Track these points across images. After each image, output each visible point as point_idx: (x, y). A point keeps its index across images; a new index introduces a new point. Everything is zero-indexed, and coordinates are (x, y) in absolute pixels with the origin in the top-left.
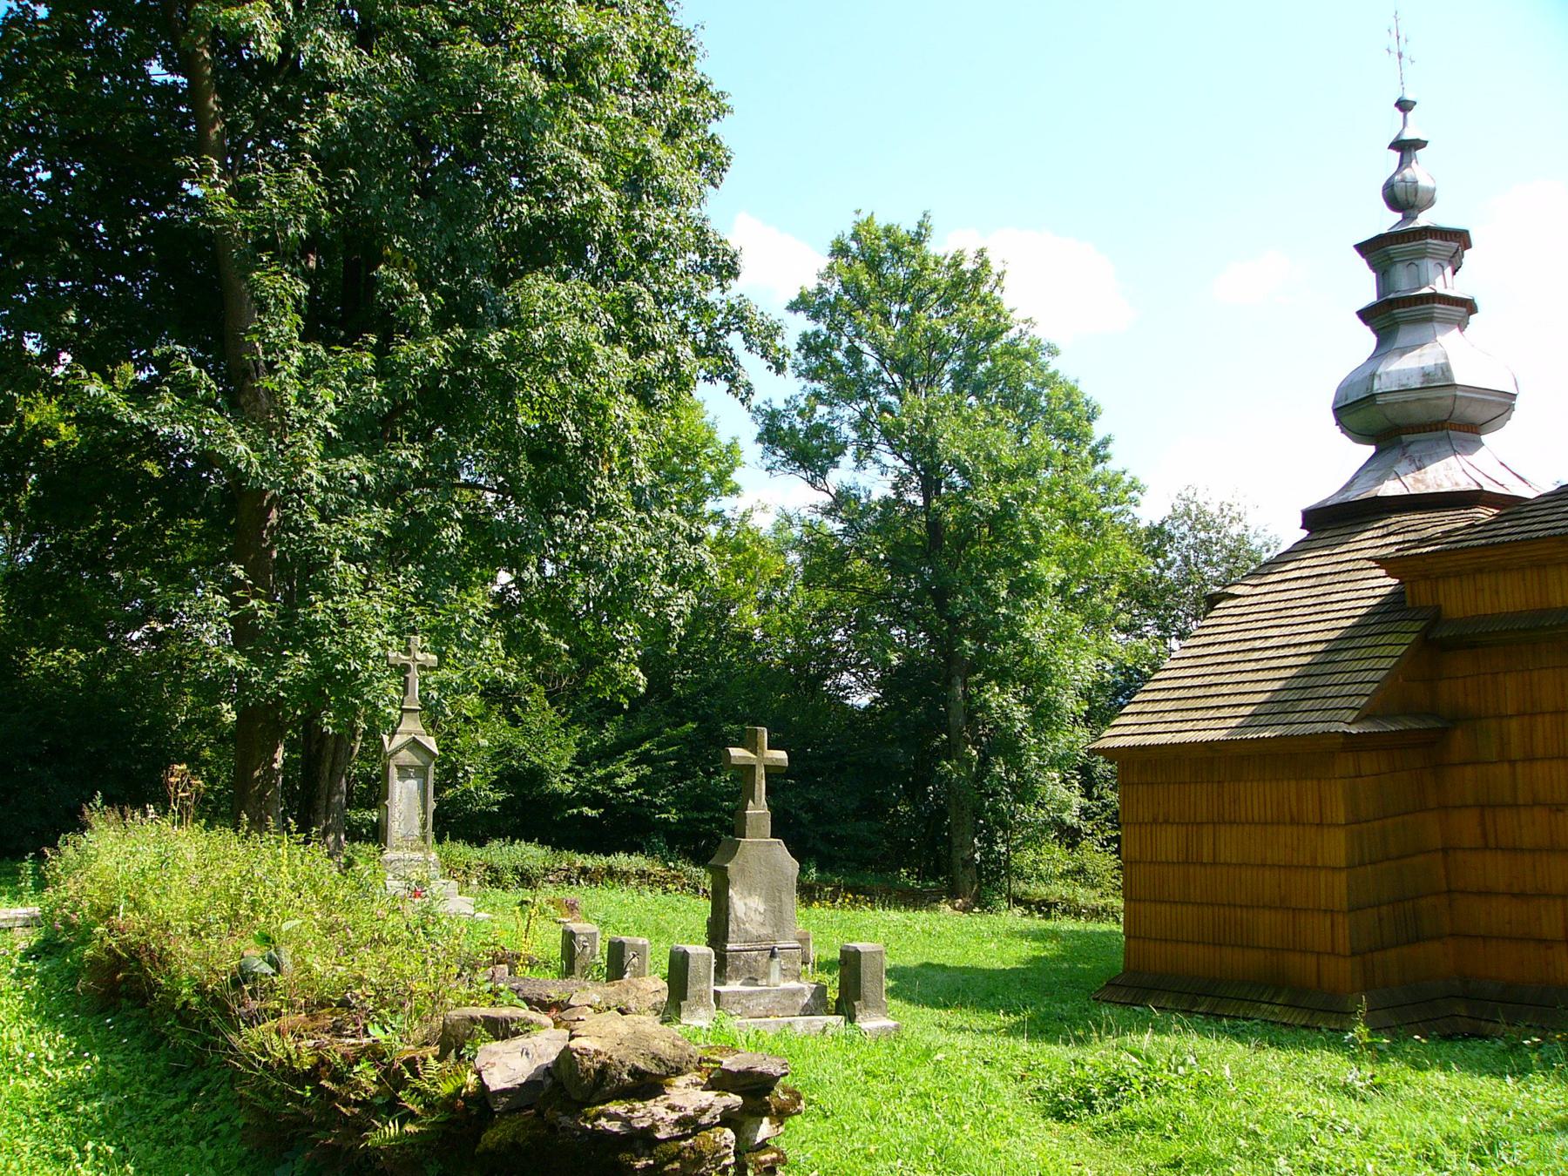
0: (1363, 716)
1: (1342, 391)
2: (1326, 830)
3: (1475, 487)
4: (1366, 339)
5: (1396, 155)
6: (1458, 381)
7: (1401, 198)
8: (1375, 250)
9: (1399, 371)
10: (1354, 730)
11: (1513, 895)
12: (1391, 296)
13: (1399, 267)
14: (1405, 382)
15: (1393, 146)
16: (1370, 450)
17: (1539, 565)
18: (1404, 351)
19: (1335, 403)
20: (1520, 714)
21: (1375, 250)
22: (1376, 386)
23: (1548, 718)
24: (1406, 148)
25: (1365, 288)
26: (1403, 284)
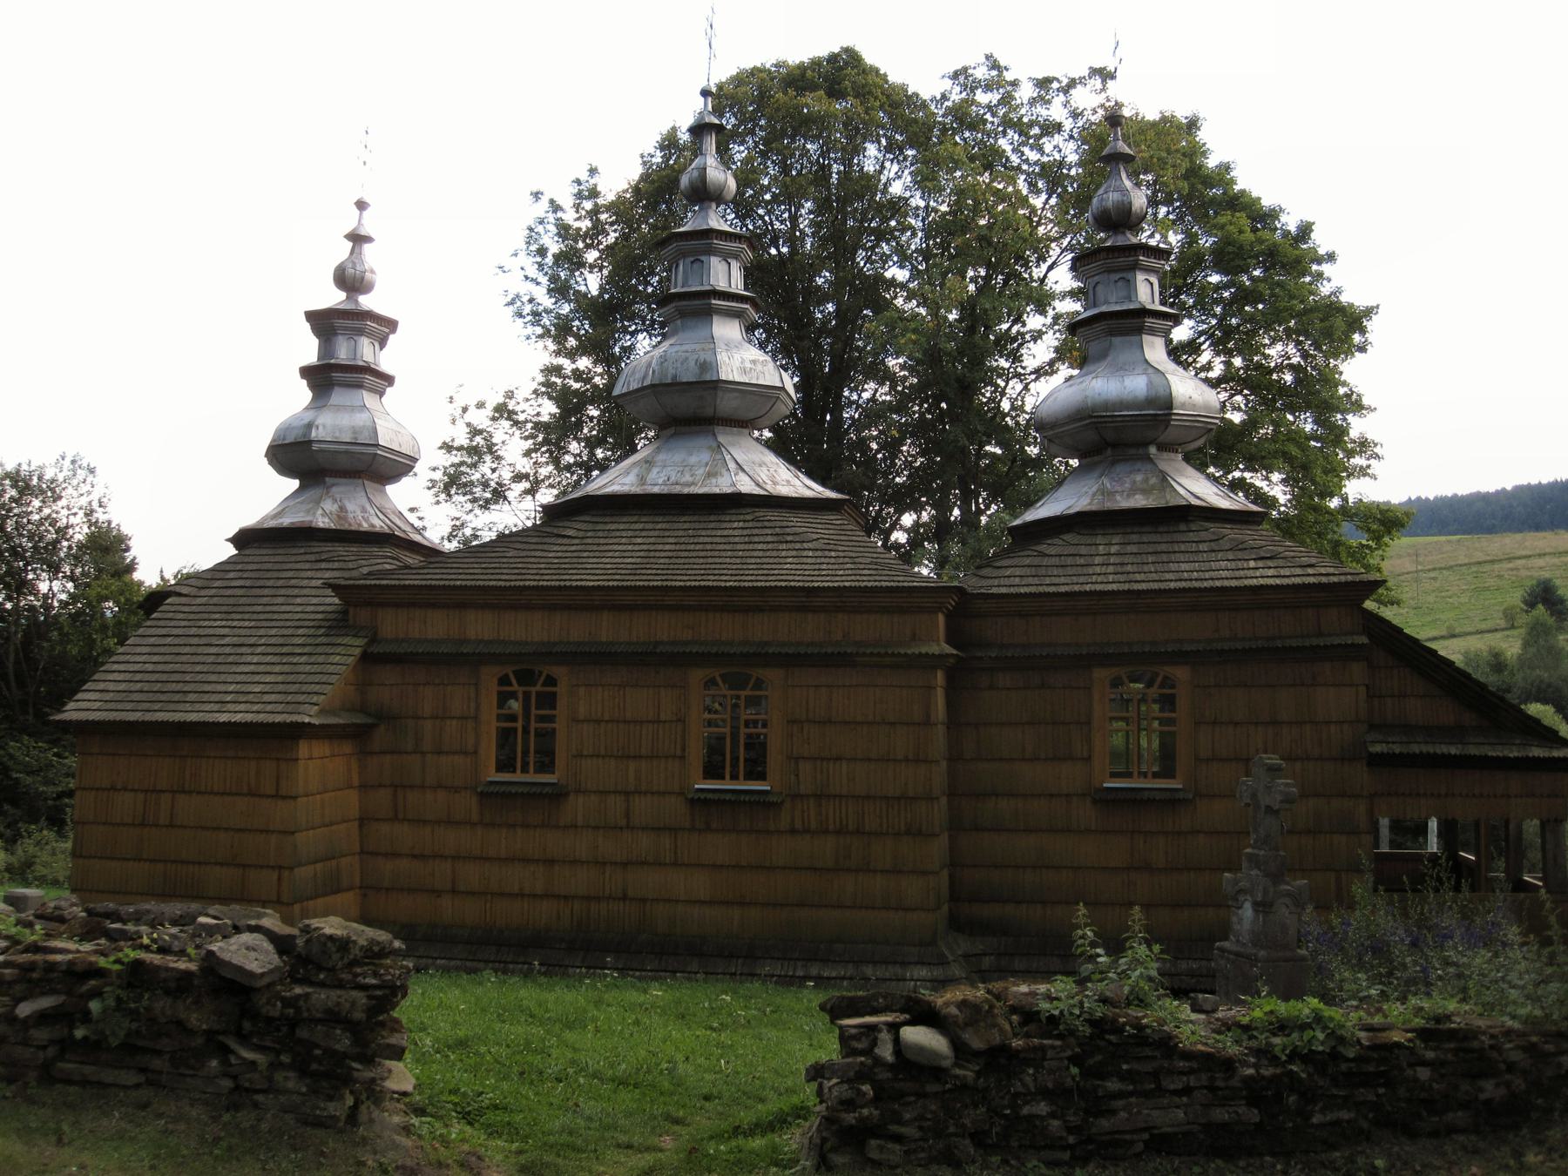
1: (282, 431)
3: (386, 530)
4: (303, 394)
7: (350, 280)
8: (324, 323)
10: (316, 721)
11: (414, 856)
12: (333, 361)
13: (340, 337)
14: (337, 434)
16: (295, 484)
17: (462, 606)
18: (339, 408)
19: (273, 440)
21: (324, 323)
22: (313, 434)
23: (454, 722)
26: (342, 354)
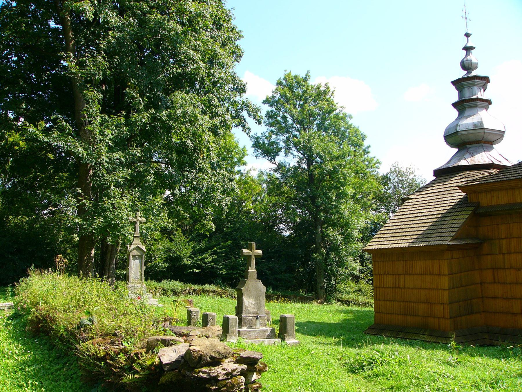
0: (454, 239)
1: (447, 130)
2: (441, 277)
3: (491, 162)
4: (455, 113)
5: (465, 52)
6: (485, 127)
7: (466, 66)
8: (458, 83)
9: (466, 124)
10: (451, 243)
11: (504, 298)
12: (463, 99)
13: (466, 89)
14: (468, 127)
15: (464, 49)
16: (456, 150)
17: (512, 188)
18: (467, 117)
19: (445, 134)
20: (506, 238)
21: (458, 83)
22: (458, 129)
23: (515, 239)
24: (468, 49)
25: (454, 96)
26: (467, 95)
